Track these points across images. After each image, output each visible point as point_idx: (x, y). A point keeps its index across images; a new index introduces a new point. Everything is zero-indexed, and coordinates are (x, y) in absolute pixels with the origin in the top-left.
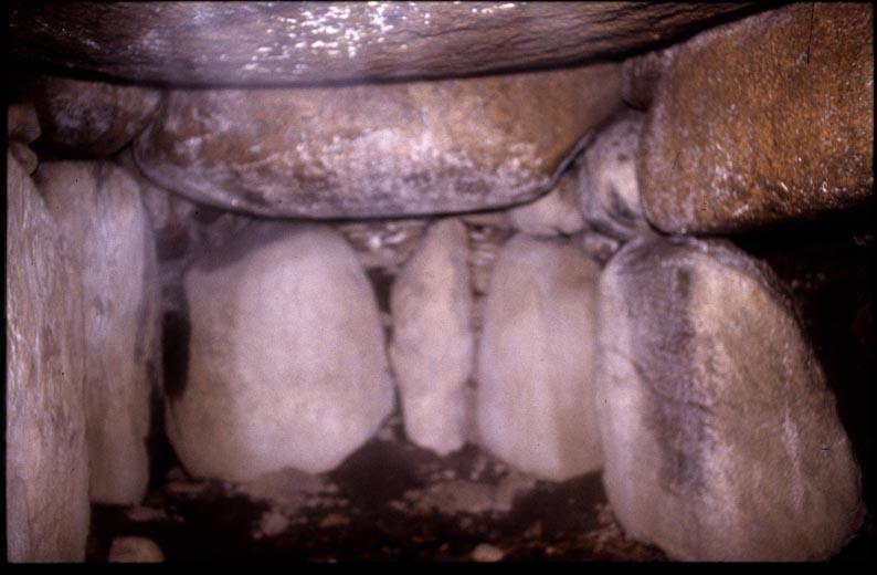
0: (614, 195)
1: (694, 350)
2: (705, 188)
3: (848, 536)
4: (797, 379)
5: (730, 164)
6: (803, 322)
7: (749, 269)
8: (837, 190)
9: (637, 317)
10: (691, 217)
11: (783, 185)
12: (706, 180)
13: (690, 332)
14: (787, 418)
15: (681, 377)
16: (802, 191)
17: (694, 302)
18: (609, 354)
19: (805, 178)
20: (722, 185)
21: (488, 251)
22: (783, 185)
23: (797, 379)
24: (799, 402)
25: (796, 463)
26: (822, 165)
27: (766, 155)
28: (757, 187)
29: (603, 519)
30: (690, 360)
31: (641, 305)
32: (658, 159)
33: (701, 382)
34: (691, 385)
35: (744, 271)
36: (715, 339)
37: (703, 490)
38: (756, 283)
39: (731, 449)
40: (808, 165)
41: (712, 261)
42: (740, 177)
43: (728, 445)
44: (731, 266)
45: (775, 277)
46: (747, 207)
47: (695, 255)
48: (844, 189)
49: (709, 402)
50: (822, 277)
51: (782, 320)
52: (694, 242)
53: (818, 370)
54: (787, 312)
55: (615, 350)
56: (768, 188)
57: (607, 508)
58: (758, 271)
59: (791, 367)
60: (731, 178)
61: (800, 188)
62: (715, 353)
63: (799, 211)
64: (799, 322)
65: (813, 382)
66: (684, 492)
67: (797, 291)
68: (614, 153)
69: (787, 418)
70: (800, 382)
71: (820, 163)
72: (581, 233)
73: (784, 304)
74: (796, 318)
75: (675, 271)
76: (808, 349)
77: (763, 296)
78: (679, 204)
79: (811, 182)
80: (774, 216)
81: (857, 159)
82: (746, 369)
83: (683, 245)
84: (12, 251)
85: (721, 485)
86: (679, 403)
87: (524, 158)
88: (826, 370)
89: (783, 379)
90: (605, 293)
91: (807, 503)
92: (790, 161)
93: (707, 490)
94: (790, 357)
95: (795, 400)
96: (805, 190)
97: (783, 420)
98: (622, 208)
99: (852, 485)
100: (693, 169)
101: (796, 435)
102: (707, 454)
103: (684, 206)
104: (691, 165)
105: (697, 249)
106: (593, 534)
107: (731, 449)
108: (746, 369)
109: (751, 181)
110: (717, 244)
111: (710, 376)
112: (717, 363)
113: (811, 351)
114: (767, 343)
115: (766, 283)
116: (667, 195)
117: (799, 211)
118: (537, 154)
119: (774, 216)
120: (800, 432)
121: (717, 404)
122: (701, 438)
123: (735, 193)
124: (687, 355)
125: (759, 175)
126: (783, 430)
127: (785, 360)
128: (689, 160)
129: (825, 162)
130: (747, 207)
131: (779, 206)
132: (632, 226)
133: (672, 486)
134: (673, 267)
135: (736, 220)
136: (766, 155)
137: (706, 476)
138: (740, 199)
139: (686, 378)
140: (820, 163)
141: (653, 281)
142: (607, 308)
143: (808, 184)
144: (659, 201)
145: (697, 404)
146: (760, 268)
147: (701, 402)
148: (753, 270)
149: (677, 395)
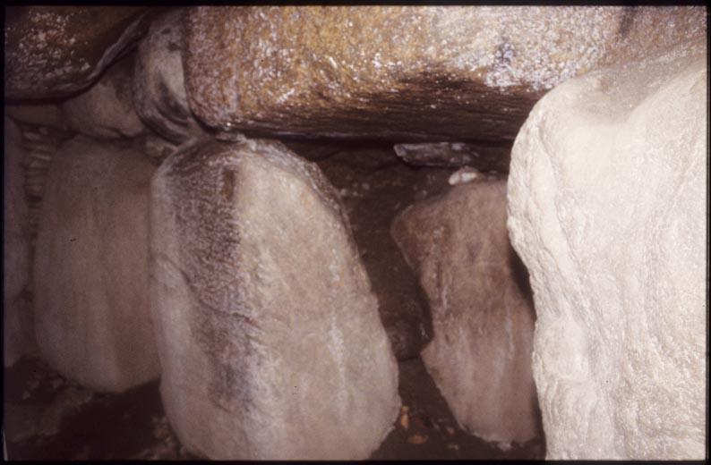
0: (163, 87)
1: (240, 259)
2: (247, 69)
3: (386, 429)
4: (344, 286)
5: (274, 35)
6: (349, 227)
7: (299, 170)
8: (391, 64)
9: (185, 222)
10: (234, 107)
11: (331, 59)
12: (248, 58)
13: (236, 238)
14: (333, 325)
15: (227, 287)
16: (352, 67)
17: (240, 204)
18: (159, 261)
19: (357, 50)
20: (265, 63)
21: (42, 152)
22: (331, 59)
23: (344, 286)
24: (345, 309)
25: (342, 370)
26: (376, 31)
27: (313, 22)
28: (304, 66)
29: (158, 433)
30: (236, 268)
31: (188, 209)
32: (201, 37)
33: (247, 293)
34: (237, 296)
35: (293, 170)
36: (261, 248)
37: (250, 407)
38: (305, 185)
39: (277, 363)
40: (360, 32)
41: (260, 158)
42: (285, 52)
43: (275, 358)
44: (280, 166)
45: (324, 181)
46: (292, 91)
47: (242, 153)
48: (399, 63)
49: (254, 314)
50: (366, 186)
51: (330, 224)
52: (242, 138)
53: (363, 275)
54: (335, 216)
55: (165, 258)
56: (315, 65)
57: (164, 420)
58: (307, 174)
59: (338, 273)
60: (275, 54)
61: (350, 63)
62: (261, 262)
63: (349, 96)
64: (346, 227)
65: (358, 288)
66: (232, 408)
67: (346, 199)
68: (163, 41)
69: (333, 325)
70: (347, 288)
71: (374, 27)
72: (141, 137)
73: (333, 209)
74: (343, 223)
75: (221, 170)
76: (354, 255)
77: (311, 198)
78: (221, 89)
79: (363, 54)
80: (322, 103)
81: (416, 22)
82: (293, 277)
83: (231, 143)
84: (527, 259)
85: (270, 400)
86: (225, 315)
87: (52, 33)
88: (370, 272)
89: (329, 286)
90: (157, 196)
91: (352, 406)
92: (339, 26)
93: (255, 406)
94: (337, 263)
95: (341, 308)
96: (356, 65)
97: (329, 328)
98: (172, 103)
99: (390, 383)
100: (235, 46)
101: (341, 341)
102: (253, 369)
103: (226, 92)
104: (233, 41)
105: (244, 146)
106: (146, 451)
107: (277, 363)
108: (293, 277)
109: (296, 57)
110: (268, 144)
111: (256, 285)
112: (263, 272)
113: (357, 257)
114: (314, 250)
115: (315, 187)
116: (209, 80)
117: (349, 96)
118: (70, 32)
119: (322, 103)
120: (345, 338)
121: (262, 317)
122: (248, 353)
123: (279, 74)
124: (232, 265)
125: (306, 49)
126: (329, 339)
127: (332, 267)
128: (231, 36)
129: (380, 27)
130: (292, 91)
131: (328, 89)
132: (185, 125)
133: (222, 401)
134: (219, 165)
135: (281, 109)
136: (313, 22)
137: (253, 391)
138: (285, 81)
139: (232, 288)
140: (374, 27)
141: (201, 183)
142: (157, 212)
143: (358, 56)
144: (202, 88)
145: (243, 316)
146: (309, 170)
147: (246, 315)
148: (303, 172)
149: (224, 308)
